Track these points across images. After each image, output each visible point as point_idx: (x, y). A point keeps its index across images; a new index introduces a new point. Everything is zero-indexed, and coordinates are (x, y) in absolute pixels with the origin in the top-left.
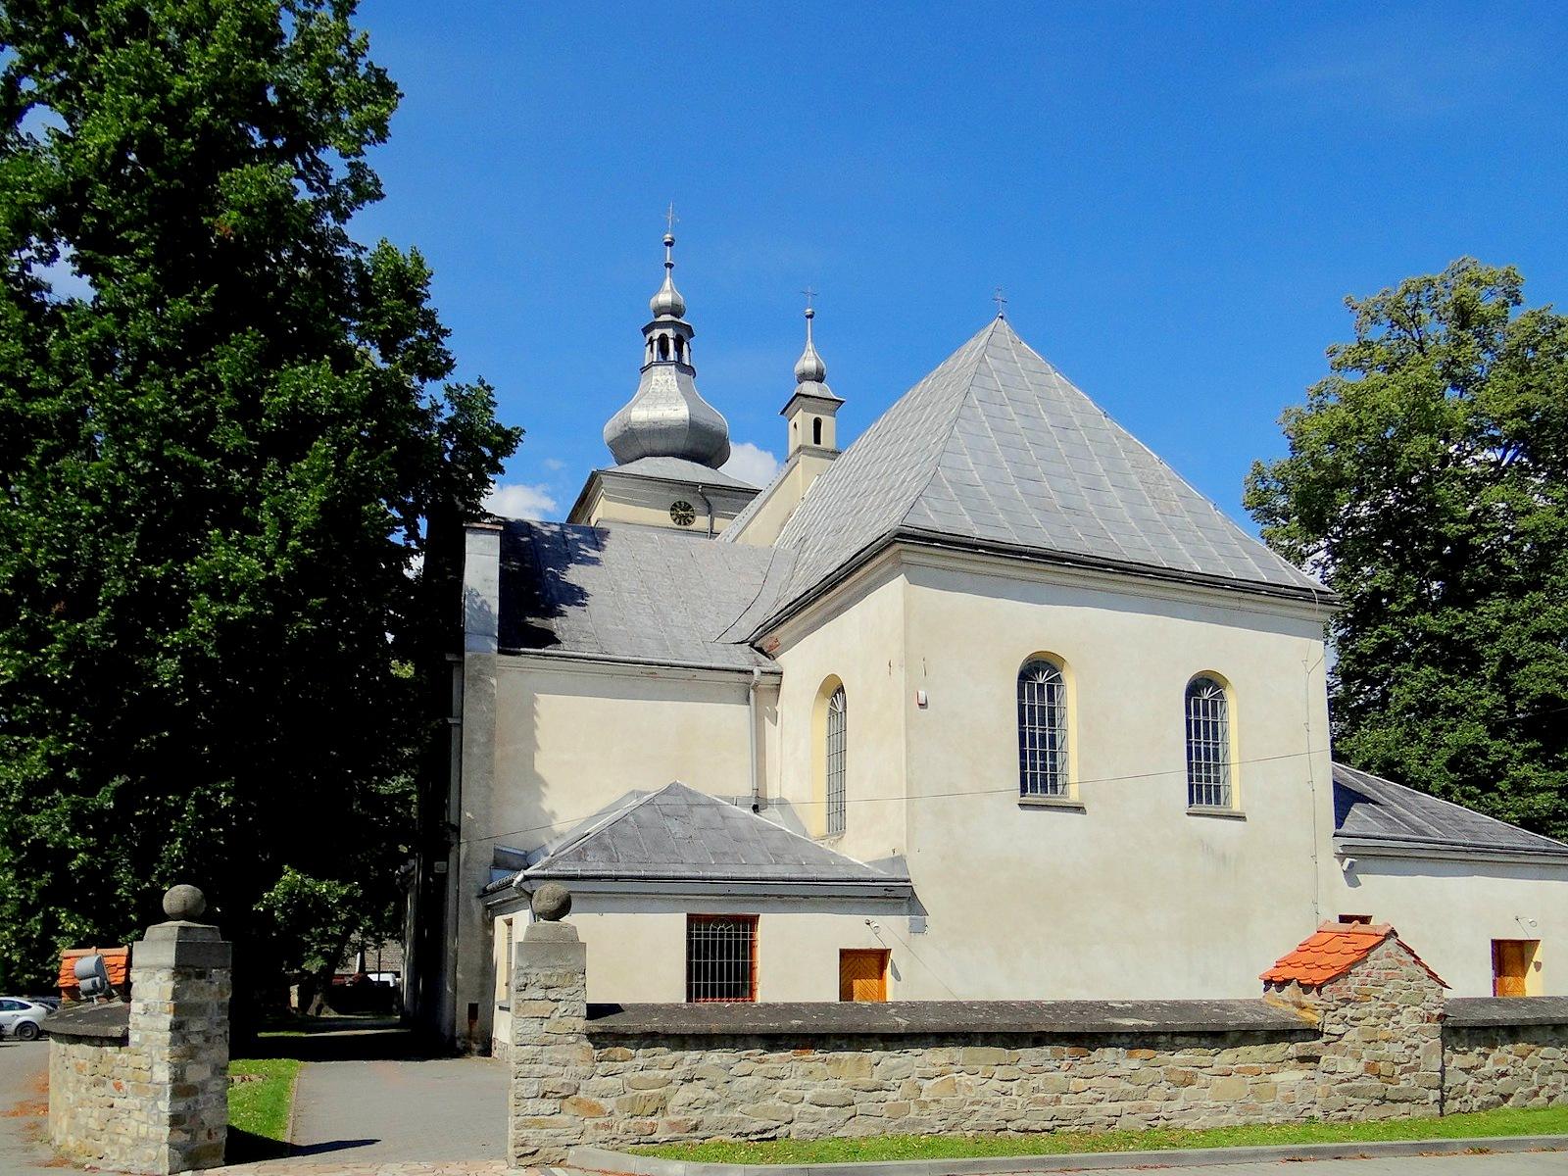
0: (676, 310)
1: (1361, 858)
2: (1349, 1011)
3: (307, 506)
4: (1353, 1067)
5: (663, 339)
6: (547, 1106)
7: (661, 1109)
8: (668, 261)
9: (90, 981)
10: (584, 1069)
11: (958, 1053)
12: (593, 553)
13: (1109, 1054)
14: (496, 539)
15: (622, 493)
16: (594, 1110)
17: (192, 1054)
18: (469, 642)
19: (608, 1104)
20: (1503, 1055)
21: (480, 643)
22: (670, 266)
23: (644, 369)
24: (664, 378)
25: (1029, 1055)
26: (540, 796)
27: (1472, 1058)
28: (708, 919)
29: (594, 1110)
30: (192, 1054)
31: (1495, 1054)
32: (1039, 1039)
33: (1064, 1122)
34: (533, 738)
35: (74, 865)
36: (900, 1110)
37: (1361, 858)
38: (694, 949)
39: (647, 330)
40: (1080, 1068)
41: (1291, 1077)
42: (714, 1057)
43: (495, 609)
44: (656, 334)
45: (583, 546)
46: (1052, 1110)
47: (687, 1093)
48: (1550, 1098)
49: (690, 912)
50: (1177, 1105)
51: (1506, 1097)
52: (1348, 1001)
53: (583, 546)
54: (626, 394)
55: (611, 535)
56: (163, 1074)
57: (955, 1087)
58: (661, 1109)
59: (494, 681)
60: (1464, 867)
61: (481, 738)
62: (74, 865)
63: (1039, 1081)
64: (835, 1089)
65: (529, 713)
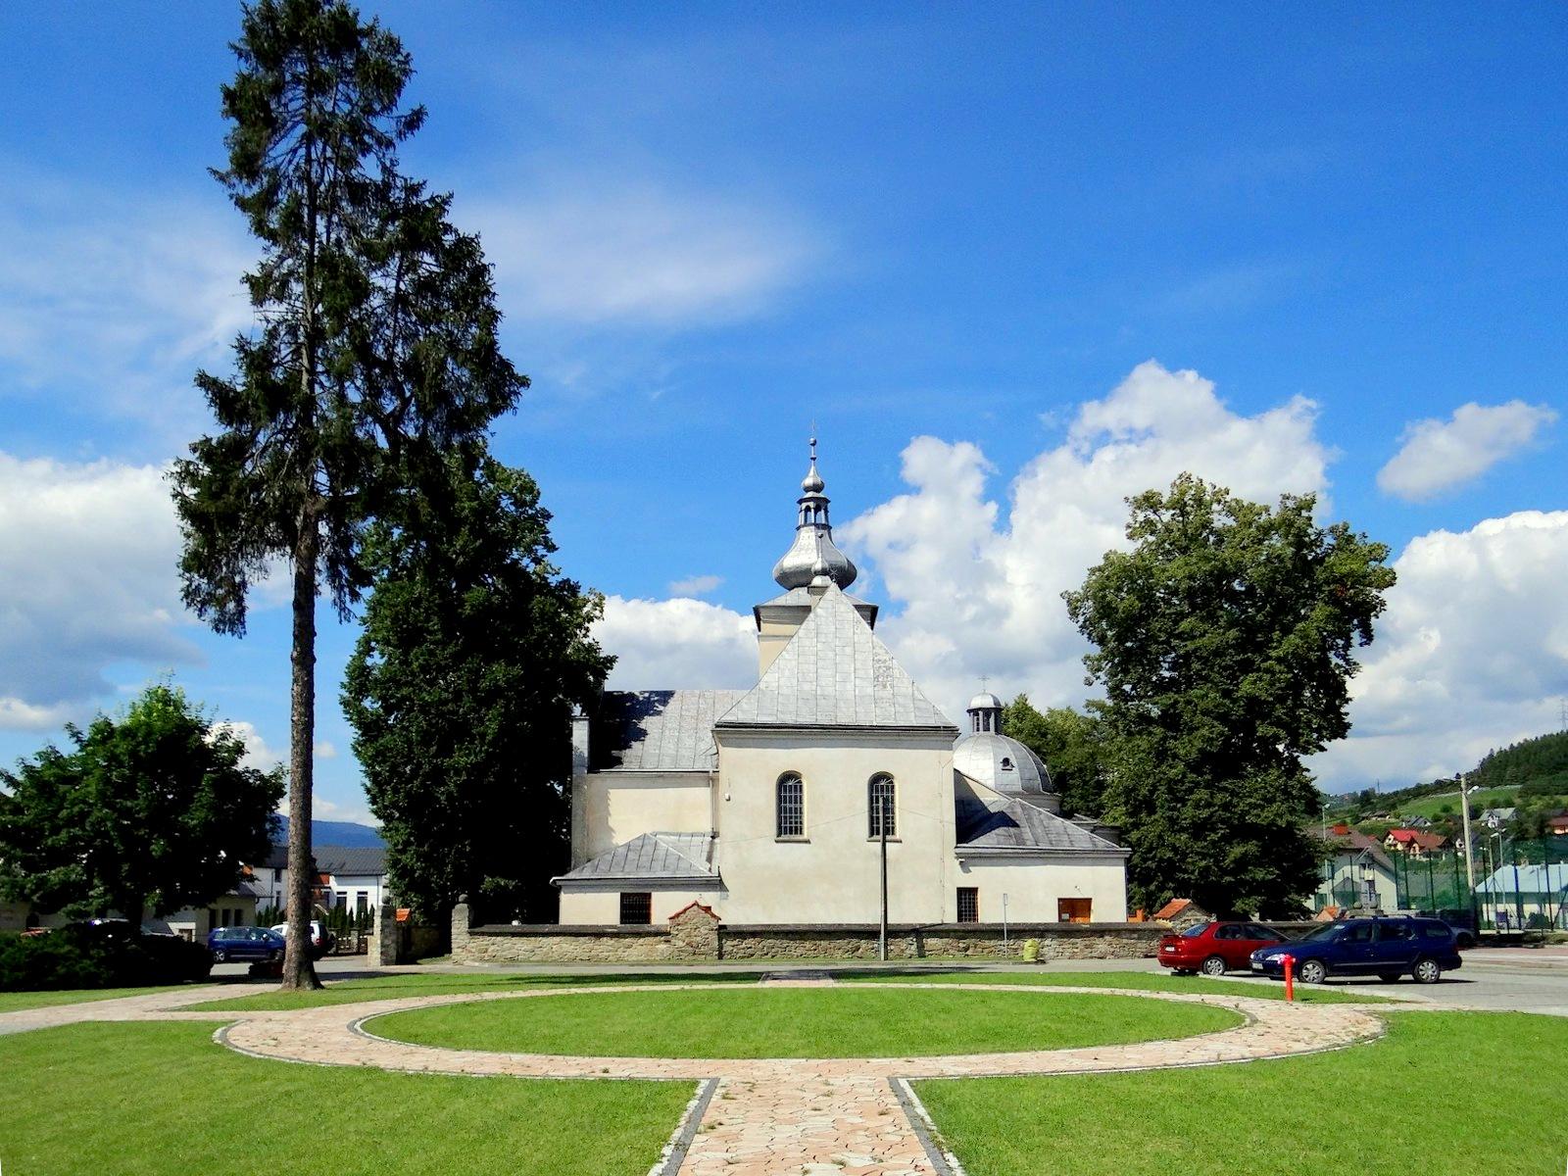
0: (817, 488)
1: (966, 862)
2: (680, 928)
3: (492, 728)
4: (681, 944)
5: (808, 509)
6: (460, 950)
7: (486, 951)
8: (813, 456)
9: (931, 962)
10: (468, 941)
11: (563, 938)
12: (661, 708)
13: (605, 939)
14: (586, 722)
15: (775, 617)
16: (470, 952)
17: (386, 937)
18: (575, 770)
19: (473, 950)
20: (750, 942)
21: (580, 772)
22: (814, 459)
23: (798, 528)
24: (808, 536)
25: (582, 939)
26: (612, 837)
27: (735, 943)
28: (629, 895)
29: (470, 952)
30: (386, 937)
31: (746, 941)
32: (584, 935)
33: (594, 957)
34: (608, 811)
35: (417, 875)
36: (547, 953)
37: (966, 862)
38: (623, 906)
39: (801, 502)
40: (597, 942)
41: (663, 946)
42: (499, 938)
43: (586, 755)
44: (804, 505)
45: (657, 704)
46: (588, 954)
47: (492, 948)
48: (773, 957)
49: (623, 891)
50: (626, 954)
51: (752, 955)
52: (679, 925)
53: (657, 704)
54: (787, 546)
55: (675, 695)
56: (379, 942)
57: (561, 948)
58: (486, 951)
59: (586, 787)
60: (1041, 861)
61: (580, 812)
62: (417, 875)
63: (585, 946)
64: (530, 947)
65: (605, 798)
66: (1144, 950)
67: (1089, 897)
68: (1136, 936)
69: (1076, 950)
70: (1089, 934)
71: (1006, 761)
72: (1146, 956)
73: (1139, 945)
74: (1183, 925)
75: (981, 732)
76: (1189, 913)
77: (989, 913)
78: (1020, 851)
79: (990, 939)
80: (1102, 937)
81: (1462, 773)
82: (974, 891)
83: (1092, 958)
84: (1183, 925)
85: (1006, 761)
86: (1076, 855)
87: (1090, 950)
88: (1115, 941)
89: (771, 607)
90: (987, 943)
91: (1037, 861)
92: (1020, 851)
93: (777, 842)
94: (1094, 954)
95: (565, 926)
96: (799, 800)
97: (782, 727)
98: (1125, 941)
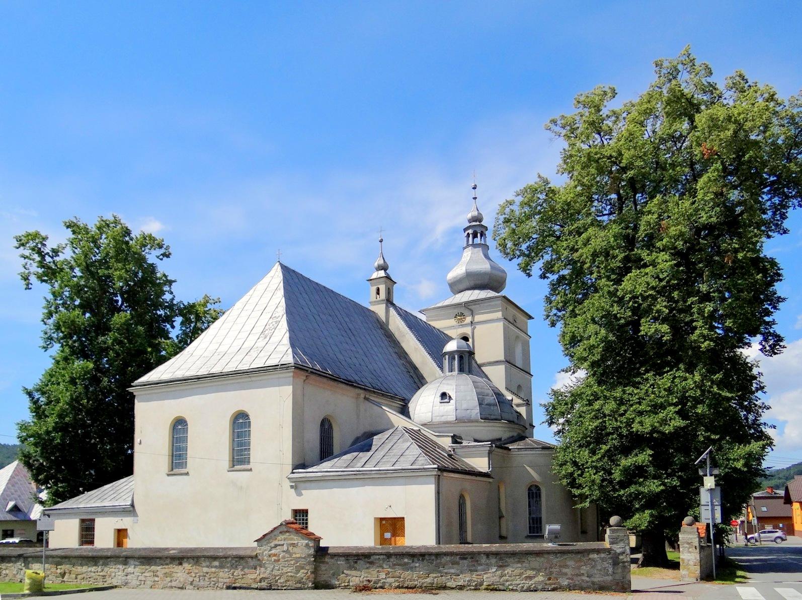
37: (297, 485)
60: (360, 482)
66: (228, 580)
67: (403, 516)
68: (216, 563)
69: (156, 579)
70: (168, 561)
71: (444, 395)
72: (228, 588)
73: (221, 574)
74: (273, 551)
75: (448, 374)
76: (282, 537)
77: (133, 542)
78: (342, 473)
79: (82, 565)
80: (181, 564)
81: (531, 340)
82: (305, 512)
83: (172, 587)
84: (273, 551)
85: (444, 395)
86: (389, 475)
87: (169, 579)
88: (195, 569)
89: (439, 308)
90: (80, 569)
91: (355, 482)
92: (342, 473)
93: (168, 475)
94: (174, 584)
95: (102, 550)
96: (185, 440)
97: (158, 383)
98: (205, 570)
